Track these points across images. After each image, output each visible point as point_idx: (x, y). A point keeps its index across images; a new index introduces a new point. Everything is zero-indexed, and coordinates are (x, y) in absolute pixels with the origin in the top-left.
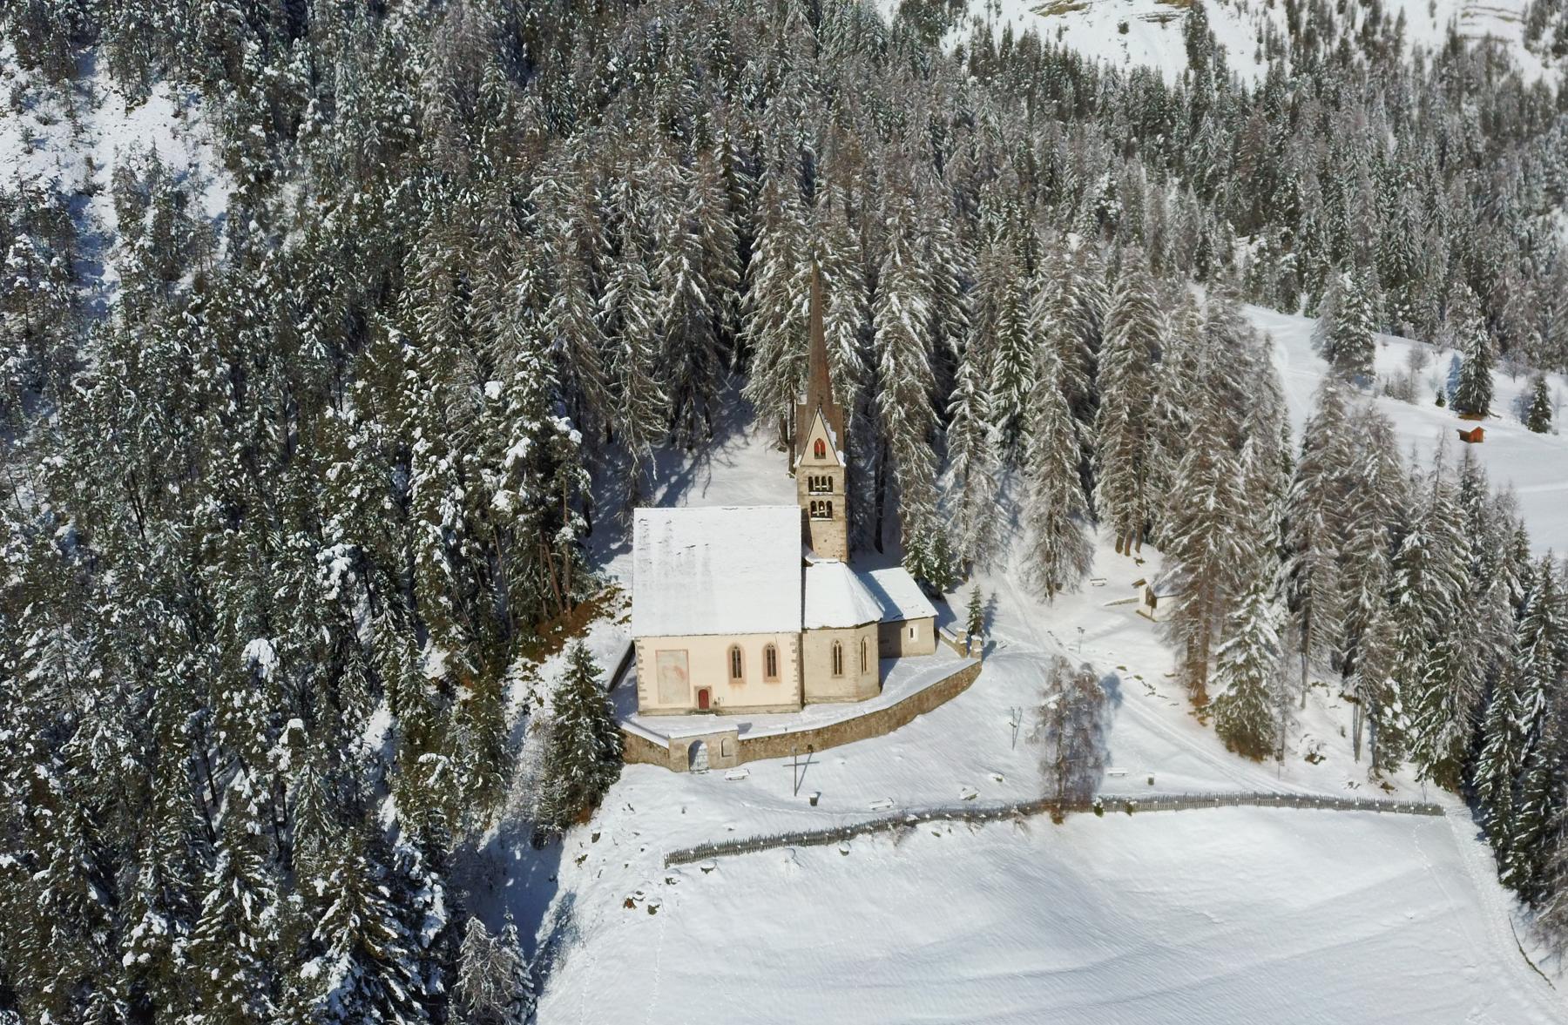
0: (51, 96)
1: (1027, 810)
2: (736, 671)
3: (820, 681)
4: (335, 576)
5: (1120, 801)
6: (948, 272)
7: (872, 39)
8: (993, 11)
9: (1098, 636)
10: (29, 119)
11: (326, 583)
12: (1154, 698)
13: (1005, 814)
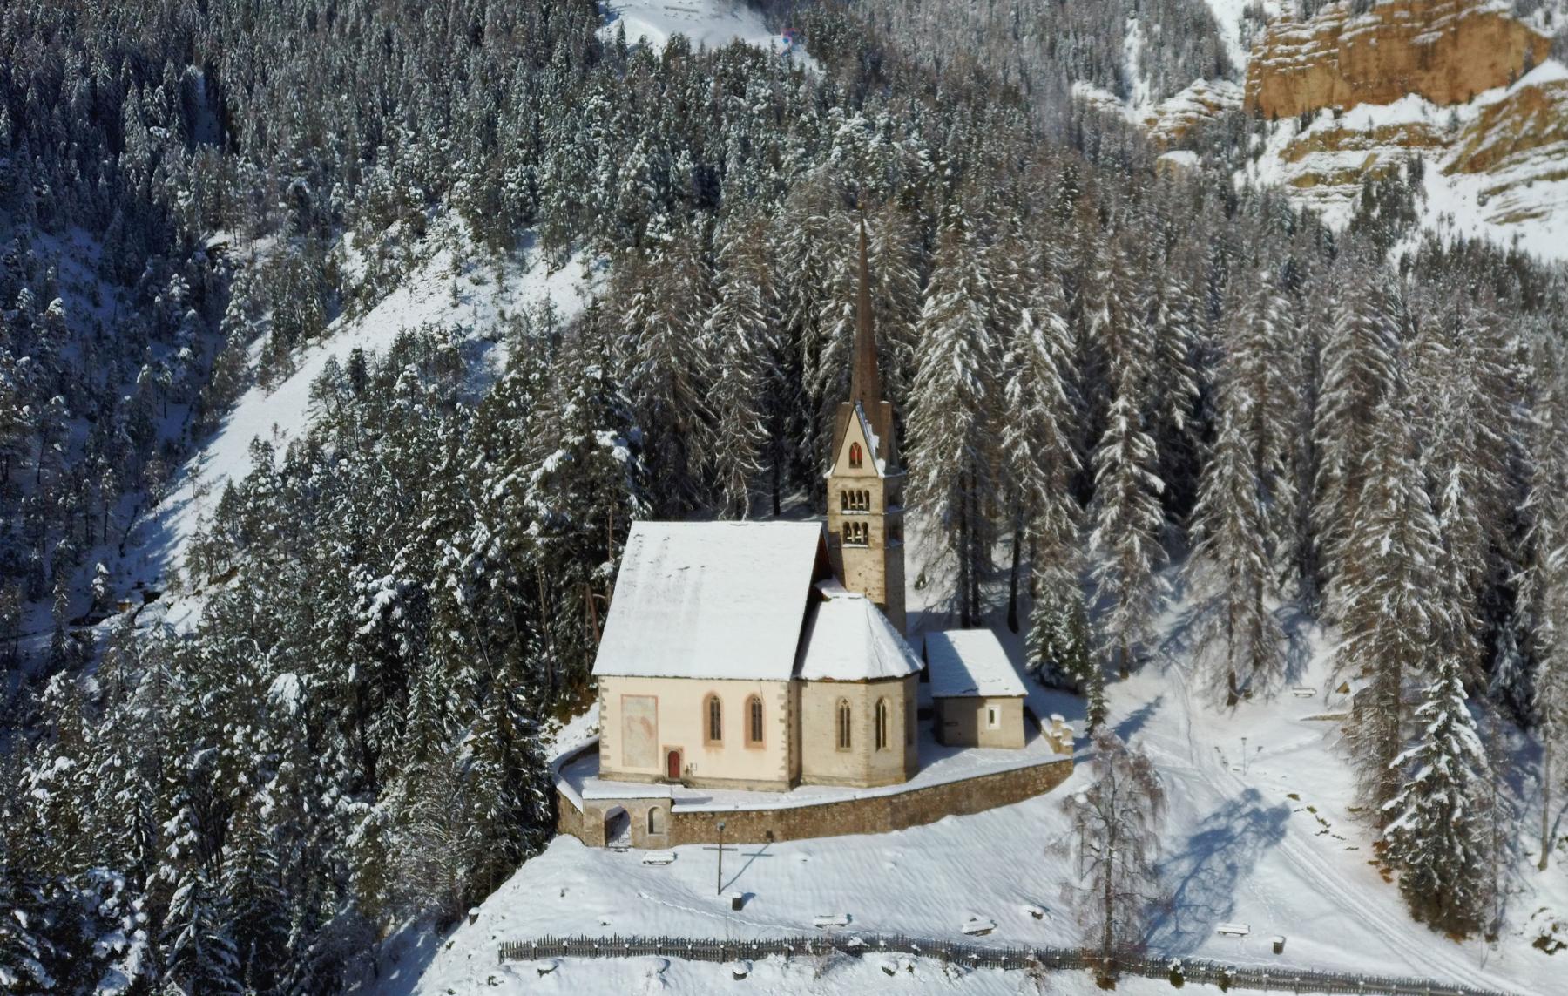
0: (489, 263)
1: (1054, 961)
2: (714, 731)
3: (820, 755)
4: (374, 610)
5: (1209, 966)
6: (1175, 335)
7: (1280, 223)
8: (1446, 224)
10: (464, 282)
11: (362, 616)
12: (1326, 838)
13: (1013, 960)
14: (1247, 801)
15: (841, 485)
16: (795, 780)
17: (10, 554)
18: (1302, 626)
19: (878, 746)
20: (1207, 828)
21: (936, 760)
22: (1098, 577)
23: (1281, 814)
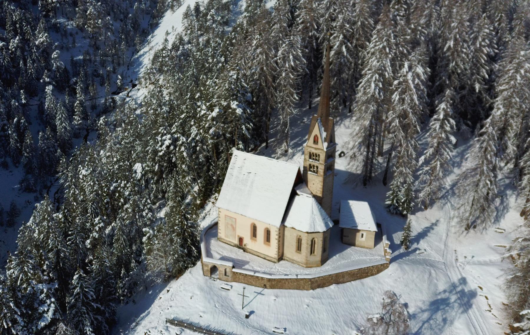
2: (254, 234)
3: (290, 251)
9: (480, 264)
11: (160, 149)
12: (490, 314)
14: (461, 284)
15: (310, 150)
16: (281, 258)
17: (95, 70)
18: (509, 192)
19: (311, 253)
20: (439, 297)
21: (335, 255)
22: (420, 174)
23: (473, 294)
